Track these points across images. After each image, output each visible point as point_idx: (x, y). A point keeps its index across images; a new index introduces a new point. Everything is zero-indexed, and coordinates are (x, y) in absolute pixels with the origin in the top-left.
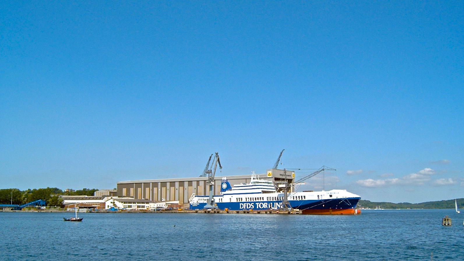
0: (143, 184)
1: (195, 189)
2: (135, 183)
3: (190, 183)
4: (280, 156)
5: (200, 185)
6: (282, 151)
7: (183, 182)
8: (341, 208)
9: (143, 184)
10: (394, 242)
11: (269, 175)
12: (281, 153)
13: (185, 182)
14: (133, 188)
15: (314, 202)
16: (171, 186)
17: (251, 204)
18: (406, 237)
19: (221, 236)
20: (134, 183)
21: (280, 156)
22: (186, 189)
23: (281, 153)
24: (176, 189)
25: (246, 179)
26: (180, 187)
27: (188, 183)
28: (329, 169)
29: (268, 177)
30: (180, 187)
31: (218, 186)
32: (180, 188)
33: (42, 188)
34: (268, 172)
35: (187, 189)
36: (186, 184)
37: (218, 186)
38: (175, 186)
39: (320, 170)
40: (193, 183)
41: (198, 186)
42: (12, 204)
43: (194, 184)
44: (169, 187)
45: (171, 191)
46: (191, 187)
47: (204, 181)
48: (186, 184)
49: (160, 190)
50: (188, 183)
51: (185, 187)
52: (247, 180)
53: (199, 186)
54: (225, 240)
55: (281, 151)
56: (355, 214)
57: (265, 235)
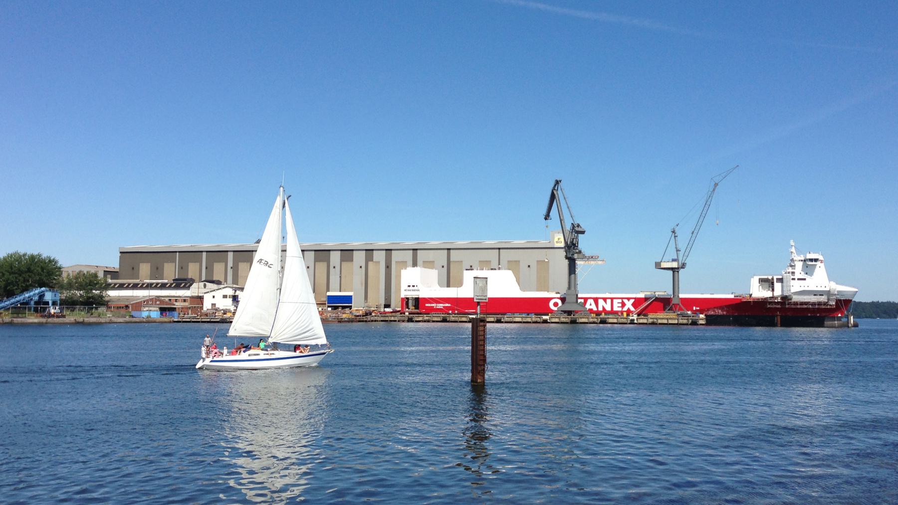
0: (230, 255)
1: (361, 267)
2: (179, 252)
3: (347, 254)
5: (375, 259)
7: (201, 253)
8: (840, 315)
9: (204, 254)
10: (656, 374)
11: (557, 242)
14: (174, 264)
15: (734, 303)
16: (343, 260)
20: (176, 252)
22: (334, 267)
24: (331, 267)
25: (499, 249)
26: (316, 263)
27: (386, 253)
28: (723, 175)
30: (342, 262)
31: (396, 262)
32: (319, 265)
33: (22, 251)
34: (556, 235)
35: (338, 268)
36: (335, 257)
37: (396, 262)
39: (712, 190)
40: (229, 255)
41: (370, 264)
42: (351, 303)
43: (359, 257)
44: (340, 261)
47: (413, 250)
48: (335, 257)
50: (339, 254)
51: (331, 263)
52: (501, 250)
56: (850, 325)
57: (865, 375)
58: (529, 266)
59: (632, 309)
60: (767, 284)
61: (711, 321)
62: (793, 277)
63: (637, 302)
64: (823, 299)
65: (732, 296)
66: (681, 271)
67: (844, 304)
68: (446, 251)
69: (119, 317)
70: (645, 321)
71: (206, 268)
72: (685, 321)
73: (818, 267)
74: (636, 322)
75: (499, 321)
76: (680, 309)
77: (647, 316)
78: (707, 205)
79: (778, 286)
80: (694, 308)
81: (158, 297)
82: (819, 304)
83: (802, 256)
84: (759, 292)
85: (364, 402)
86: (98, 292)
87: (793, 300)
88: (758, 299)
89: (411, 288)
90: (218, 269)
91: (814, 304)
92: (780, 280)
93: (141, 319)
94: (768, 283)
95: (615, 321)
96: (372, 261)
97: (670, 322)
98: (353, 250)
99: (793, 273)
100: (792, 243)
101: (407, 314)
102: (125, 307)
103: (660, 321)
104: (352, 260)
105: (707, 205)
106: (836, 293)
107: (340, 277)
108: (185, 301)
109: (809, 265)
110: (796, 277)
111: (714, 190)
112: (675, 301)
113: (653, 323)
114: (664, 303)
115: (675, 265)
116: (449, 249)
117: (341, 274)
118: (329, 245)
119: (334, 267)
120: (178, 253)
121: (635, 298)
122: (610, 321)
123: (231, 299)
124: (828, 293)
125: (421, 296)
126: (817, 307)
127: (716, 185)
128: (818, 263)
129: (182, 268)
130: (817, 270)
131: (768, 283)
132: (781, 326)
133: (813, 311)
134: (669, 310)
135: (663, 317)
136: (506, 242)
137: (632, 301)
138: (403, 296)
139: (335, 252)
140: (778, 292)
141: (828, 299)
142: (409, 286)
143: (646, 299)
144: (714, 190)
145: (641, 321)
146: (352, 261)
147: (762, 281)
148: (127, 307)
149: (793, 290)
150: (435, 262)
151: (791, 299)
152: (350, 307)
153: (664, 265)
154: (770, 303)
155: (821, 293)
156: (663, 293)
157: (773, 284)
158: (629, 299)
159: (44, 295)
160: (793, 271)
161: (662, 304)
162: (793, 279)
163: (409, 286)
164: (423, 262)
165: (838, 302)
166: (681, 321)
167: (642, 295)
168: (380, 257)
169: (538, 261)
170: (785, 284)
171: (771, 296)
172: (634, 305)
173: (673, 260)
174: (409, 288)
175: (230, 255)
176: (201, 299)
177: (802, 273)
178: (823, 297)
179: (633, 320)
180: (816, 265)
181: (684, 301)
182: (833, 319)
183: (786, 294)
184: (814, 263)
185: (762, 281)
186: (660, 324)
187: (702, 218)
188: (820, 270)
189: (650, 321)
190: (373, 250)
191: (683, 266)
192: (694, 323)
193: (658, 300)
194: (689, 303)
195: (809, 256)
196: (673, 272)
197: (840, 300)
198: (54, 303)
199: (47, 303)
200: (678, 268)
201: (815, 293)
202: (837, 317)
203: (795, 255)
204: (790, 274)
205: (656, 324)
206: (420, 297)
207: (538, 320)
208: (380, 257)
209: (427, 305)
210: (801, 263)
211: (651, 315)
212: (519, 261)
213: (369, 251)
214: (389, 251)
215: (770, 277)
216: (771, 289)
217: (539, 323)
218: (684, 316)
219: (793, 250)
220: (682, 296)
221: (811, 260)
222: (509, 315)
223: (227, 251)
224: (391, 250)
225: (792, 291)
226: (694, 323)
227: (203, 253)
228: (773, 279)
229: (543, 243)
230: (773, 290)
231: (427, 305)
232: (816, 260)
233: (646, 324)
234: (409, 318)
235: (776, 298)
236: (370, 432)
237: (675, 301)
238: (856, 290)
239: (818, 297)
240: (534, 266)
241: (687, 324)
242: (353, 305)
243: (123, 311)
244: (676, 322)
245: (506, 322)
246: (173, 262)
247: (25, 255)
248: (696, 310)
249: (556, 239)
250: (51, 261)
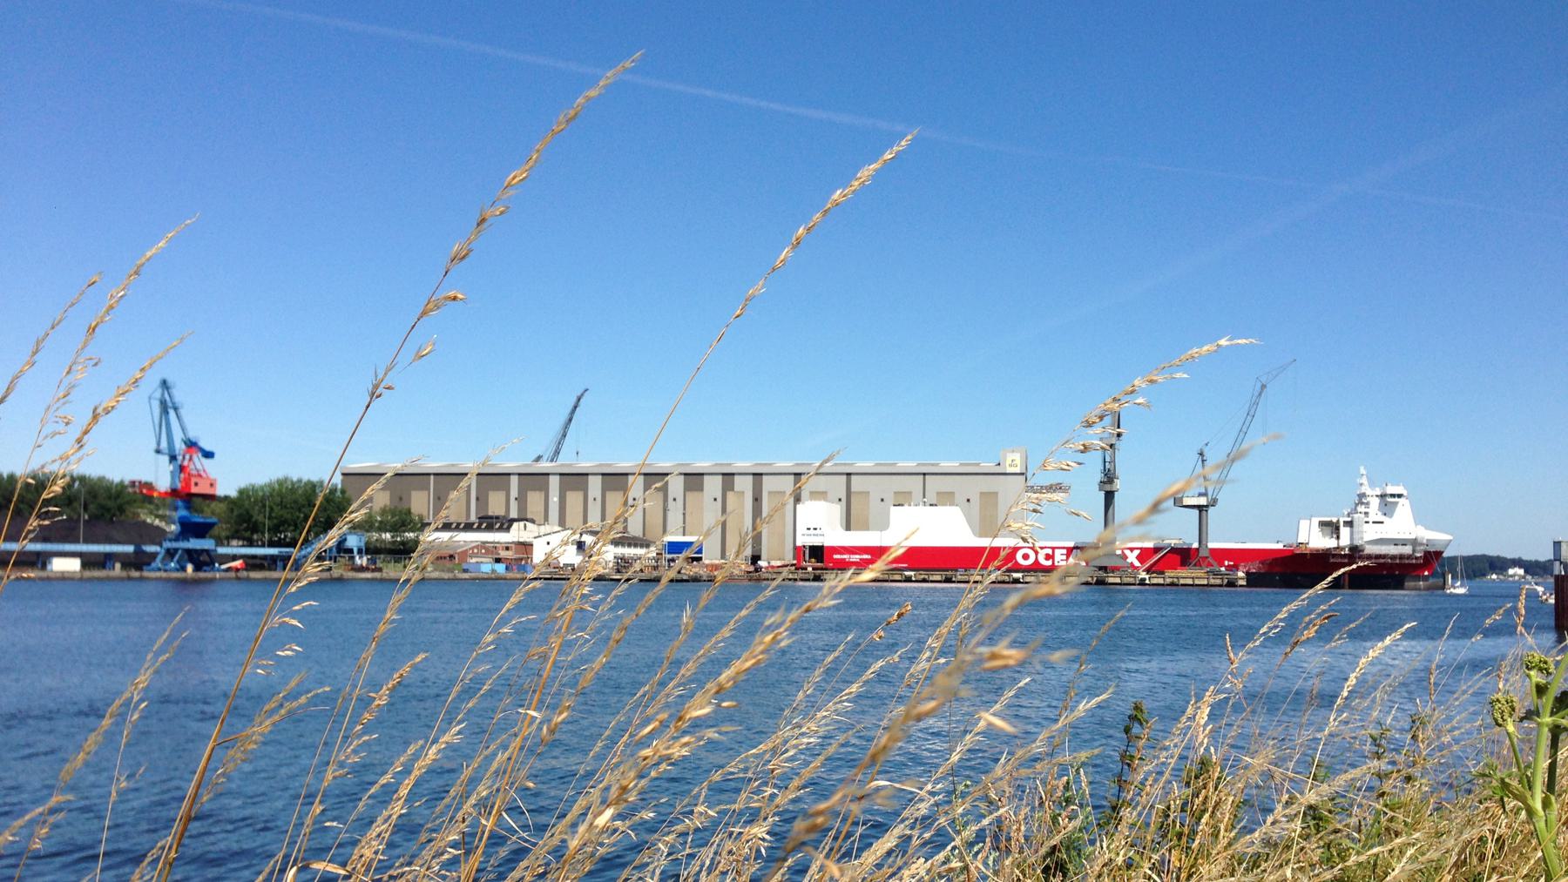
0: (514, 480)
1: (715, 500)
2: (435, 474)
3: (694, 480)
4: (575, 407)
5: (737, 488)
6: (582, 395)
8: (1426, 573)
12: (579, 399)
13: (736, 477)
14: (427, 492)
17: (1037, 561)
18: (601, 782)
19: (291, 796)
20: (429, 474)
21: (575, 407)
22: (675, 500)
23: (579, 399)
25: (924, 474)
26: (687, 493)
27: (603, 483)
29: (1010, 470)
30: (687, 493)
32: (610, 496)
36: (676, 485)
38: (585, 490)
39: (1257, 394)
41: (730, 495)
43: (713, 486)
45: (582, 514)
46: (696, 494)
47: (795, 474)
49: (556, 499)
52: (927, 477)
53: (732, 489)
54: (1008, 768)
55: (579, 394)
58: (968, 500)
59: (1137, 564)
60: (1328, 529)
61: (1253, 580)
62: (1366, 519)
63: (1144, 554)
64: (1407, 550)
65: (1280, 546)
66: (1211, 510)
67: (1432, 558)
68: (792, 477)
69: (443, 571)
70: (1161, 581)
71: (477, 499)
72: (1218, 582)
73: (1400, 505)
74: (1147, 582)
75: (948, 580)
76: (1210, 565)
77: (1163, 573)
78: (1250, 414)
79: (1345, 532)
80: (1226, 563)
81: (484, 543)
82: (1401, 557)
83: (1377, 489)
84: (1319, 541)
85: (256, 772)
86: (412, 535)
87: (1366, 552)
88: (1318, 550)
89: (812, 531)
90: (535, 499)
91: (1393, 557)
92: (1350, 524)
93: (481, 575)
94: (1332, 528)
95: (1118, 580)
96: (733, 490)
97: (1197, 582)
98: (703, 474)
99: (1366, 513)
100: (1362, 470)
101: (810, 569)
102: (448, 558)
103: (1182, 581)
104: (702, 490)
105: (1250, 414)
106: (1425, 541)
107: (684, 514)
108: (507, 549)
109: (1388, 503)
110: (1371, 519)
111: (1260, 394)
112: (1203, 553)
113: (1172, 584)
114: (1184, 556)
115: (1203, 501)
116: (849, 474)
117: (684, 509)
118: (623, 465)
119: (675, 500)
120: (432, 477)
121: (1141, 549)
122: (1111, 580)
123: (575, 547)
124: (1414, 542)
125: (826, 544)
126: (1398, 561)
127: (1264, 386)
128: (1401, 501)
129: (439, 498)
130: (1399, 509)
131: (1332, 528)
132: (1350, 588)
133: (1391, 567)
134: (1195, 565)
135: (1186, 575)
136: (933, 465)
137: (1137, 552)
138: (804, 540)
139: (711, 477)
140: (1345, 540)
141: (1414, 551)
142: (809, 529)
143: (1156, 550)
144: (1260, 394)
145: (1155, 581)
146: (702, 490)
147: (1323, 524)
148: (452, 557)
149: (1367, 537)
150: (957, 495)
151: (1363, 551)
152: (700, 559)
153: (1187, 501)
154: (1334, 556)
155: (1404, 543)
156: (1177, 542)
157: (1337, 528)
158: (1132, 549)
159: (345, 540)
160: (1367, 510)
161: (1179, 557)
162: (1367, 522)
163: (809, 529)
164: (938, 493)
165: (1428, 555)
166: (1212, 581)
167: (1150, 545)
168: (744, 485)
169: (981, 493)
170: (1355, 529)
171: (1336, 546)
172: (1138, 558)
173: (1200, 495)
174: (809, 532)
175: (514, 480)
176: (526, 547)
177: (1380, 513)
178: (1407, 547)
179: (1145, 579)
180: (1397, 503)
181: (1213, 551)
182: (1418, 578)
183: (1358, 542)
184: (1396, 499)
185: (1323, 524)
186: (1182, 585)
187: (1242, 435)
188: (1404, 508)
189: (1168, 581)
190: (733, 474)
191: (1214, 503)
192: (1231, 584)
193: (1174, 551)
194: (1220, 555)
195: (1390, 490)
196: (1200, 511)
197: (1429, 552)
198: (360, 551)
199: (351, 551)
200: (1207, 506)
201: (1396, 542)
202: (1423, 576)
203: (1367, 487)
204: (1363, 515)
205: (1177, 585)
206: (825, 545)
207: (1006, 578)
208: (744, 485)
209: (836, 556)
210: (1377, 500)
211: (1169, 573)
212: (996, 493)
213: (728, 477)
214: (758, 476)
215: (1335, 520)
216: (1335, 536)
217: (1008, 583)
218: (1216, 574)
219: (1364, 480)
220: (1211, 545)
221: (1393, 496)
222: (961, 571)
223: (509, 474)
224: (761, 474)
225: (1365, 540)
226: (1231, 584)
227: (512, 477)
228: (1338, 521)
229: (988, 466)
230: (1338, 538)
231: (836, 556)
232: (1400, 496)
233: (1163, 585)
234: (815, 576)
235: (1343, 549)
236: (1146, 684)
237: (1203, 553)
238: (1450, 537)
239: (1400, 547)
240: (975, 499)
241: (1220, 586)
242: (703, 555)
243: (448, 564)
244: (1205, 582)
245: (959, 582)
246: (540, 490)
247: (300, 481)
248: (1229, 566)
249: (1009, 462)
250: (281, 483)
